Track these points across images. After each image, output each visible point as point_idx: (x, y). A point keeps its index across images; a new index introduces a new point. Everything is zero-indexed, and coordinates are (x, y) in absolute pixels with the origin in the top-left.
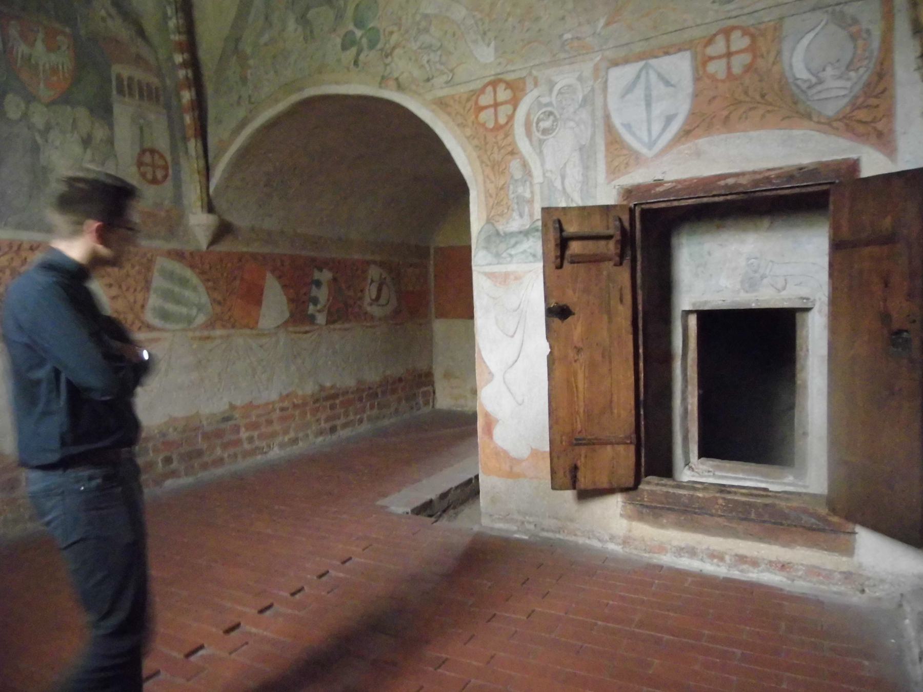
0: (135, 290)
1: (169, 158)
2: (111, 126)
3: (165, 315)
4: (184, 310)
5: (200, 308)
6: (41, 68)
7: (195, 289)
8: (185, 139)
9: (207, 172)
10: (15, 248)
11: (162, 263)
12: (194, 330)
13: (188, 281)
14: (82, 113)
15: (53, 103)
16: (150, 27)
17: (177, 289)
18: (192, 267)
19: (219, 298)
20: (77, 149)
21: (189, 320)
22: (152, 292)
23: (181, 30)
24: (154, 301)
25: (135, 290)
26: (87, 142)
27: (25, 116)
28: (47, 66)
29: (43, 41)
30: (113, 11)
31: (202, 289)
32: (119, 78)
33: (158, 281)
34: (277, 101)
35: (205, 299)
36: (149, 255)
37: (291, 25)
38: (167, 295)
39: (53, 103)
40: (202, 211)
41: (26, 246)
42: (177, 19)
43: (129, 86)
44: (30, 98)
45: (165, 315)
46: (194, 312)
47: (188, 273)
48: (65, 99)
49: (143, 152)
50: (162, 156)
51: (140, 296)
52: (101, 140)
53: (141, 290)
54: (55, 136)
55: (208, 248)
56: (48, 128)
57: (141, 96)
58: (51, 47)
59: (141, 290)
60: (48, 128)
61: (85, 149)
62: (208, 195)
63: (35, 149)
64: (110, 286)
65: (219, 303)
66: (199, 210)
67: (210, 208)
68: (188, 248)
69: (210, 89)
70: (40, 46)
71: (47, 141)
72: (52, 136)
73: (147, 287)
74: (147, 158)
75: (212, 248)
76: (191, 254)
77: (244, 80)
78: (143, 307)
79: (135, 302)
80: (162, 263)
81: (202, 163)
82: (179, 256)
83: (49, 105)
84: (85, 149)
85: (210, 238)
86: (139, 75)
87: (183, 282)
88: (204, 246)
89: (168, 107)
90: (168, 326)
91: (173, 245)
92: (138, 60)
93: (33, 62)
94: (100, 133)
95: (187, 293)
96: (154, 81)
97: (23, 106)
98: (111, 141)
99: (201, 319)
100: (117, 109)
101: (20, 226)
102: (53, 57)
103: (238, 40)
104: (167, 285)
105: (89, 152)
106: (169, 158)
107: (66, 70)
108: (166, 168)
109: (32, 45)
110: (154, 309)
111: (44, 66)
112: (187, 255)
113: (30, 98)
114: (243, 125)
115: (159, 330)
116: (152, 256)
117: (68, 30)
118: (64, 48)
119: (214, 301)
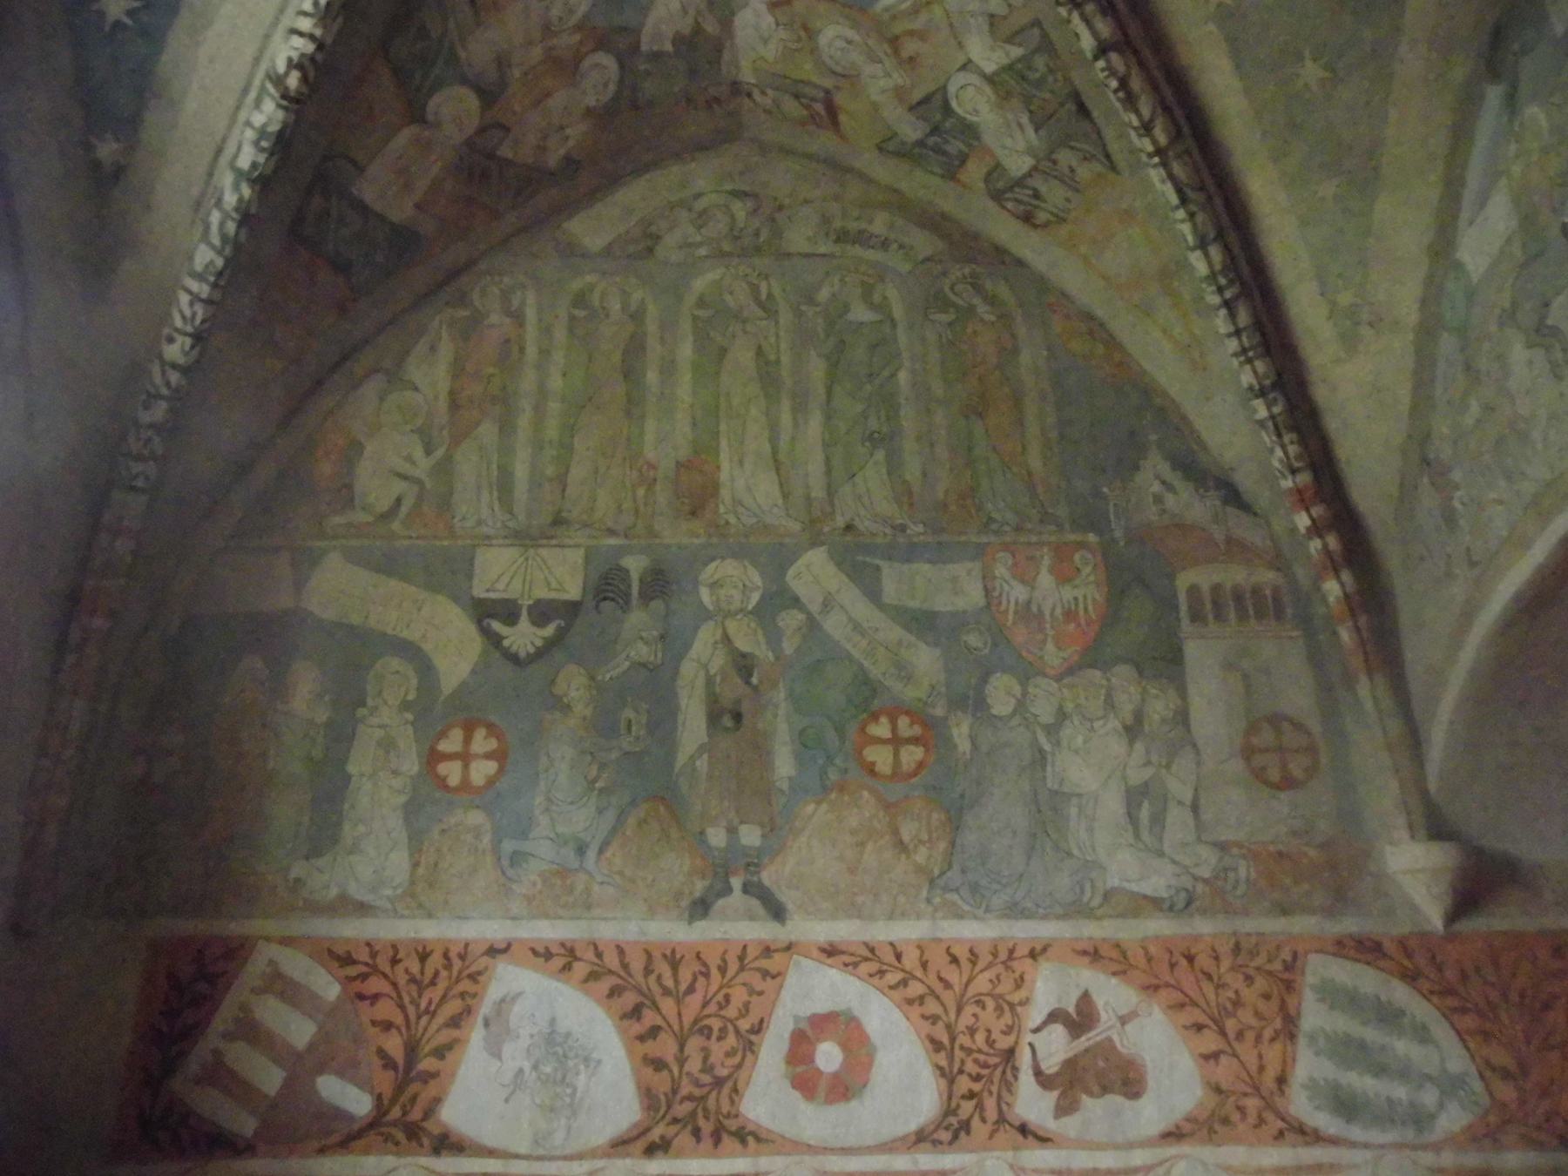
0: (1258, 1038)
1: (1315, 726)
2: (1182, 692)
3: (1346, 1105)
4: (1400, 1092)
5: (1451, 1086)
6: (1048, 617)
7: (1422, 1035)
8: (1349, 681)
9: (1414, 740)
10: (1003, 956)
11: (1321, 969)
12: (1437, 1147)
13: (1401, 1013)
14: (1123, 673)
15: (1071, 671)
16: (1246, 481)
17: (1371, 1035)
18: (1410, 977)
19: (1502, 1058)
20: (1117, 746)
21: (1419, 1119)
22: (1302, 1041)
23: (1297, 465)
24: (1308, 1066)
25: (1258, 1038)
26: (1133, 731)
27: (1021, 705)
28: (1058, 611)
29: (1051, 570)
30: (1174, 478)
31: (1442, 1031)
32: (1193, 591)
33: (1314, 1016)
34: (1526, 544)
35: (1457, 1060)
36: (1286, 955)
37: (1519, 353)
38: (1349, 1051)
39: (1071, 671)
40: (1413, 837)
41: (1022, 951)
42: (1283, 447)
43: (1215, 603)
44: (1027, 672)
45: (1346, 1105)
46: (1429, 1097)
47: (1400, 994)
48: (1093, 657)
49: (1252, 729)
50: (1298, 726)
51: (1273, 1054)
52: (1164, 721)
53: (1273, 1040)
54: (1073, 733)
55: (1453, 916)
56: (1062, 716)
57: (1243, 616)
58: (1064, 576)
59: (1273, 1040)
60: (1062, 716)
61: (1131, 742)
62: (1424, 793)
63: (1040, 759)
64: (1199, 1027)
65: (1506, 1075)
66: (1404, 834)
67: (1437, 828)
68: (1387, 930)
69: (1392, 556)
70: (1045, 580)
71: (1058, 743)
72: (1066, 732)
73: (1289, 1028)
74: (1266, 737)
75: (1466, 926)
76: (1402, 943)
77: (1450, 518)
78: (1282, 1081)
79: (1261, 1068)
80: (1321, 969)
81: (1395, 726)
82: (1367, 949)
83: (1059, 679)
84: (1131, 742)
85: (1448, 901)
86: (1235, 575)
87: (1389, 1016)
88: (1435, 918)
89: (1305, 621)
90: (1356, 1133)
91: (1349, 925)
92: (1235, 549)
93: (1034, 609)
94: (1160, 707)
95: (1402, 1046)
96: (1268, 577)
97: (1017, 690)
98: (1182, 717)
99: (1453, 1119)
100: (1192, 650)
101: (1014, 911)
102: (1068, 593)
103: (1427, 438)
104: (1342, 1023)
105: (1139, 747)
106: (1315, 726)
107: (1090, 608)
108: (1312, 750)
109: (1029, 582)
110: (1312, 1086)
111: (1053, 609)
112: (1388, 946)
113: (1027, 672)
114: (1468, 614)
115: (1334, 1141)
116: (1295, 955)
117: (1092, 538)
118: (1087, 570)
119: (1488, 1069)
